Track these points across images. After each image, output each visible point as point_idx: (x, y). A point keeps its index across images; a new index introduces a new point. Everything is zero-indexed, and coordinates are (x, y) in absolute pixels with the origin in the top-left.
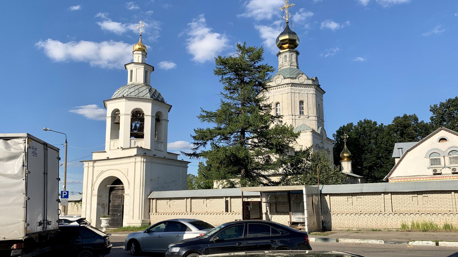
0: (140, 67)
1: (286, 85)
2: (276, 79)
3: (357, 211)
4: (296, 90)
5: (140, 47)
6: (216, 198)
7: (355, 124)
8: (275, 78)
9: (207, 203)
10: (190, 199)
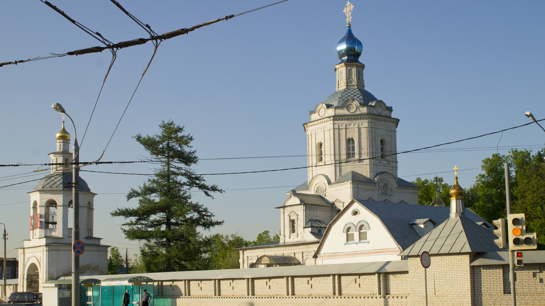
0: (60, 156)
1: (327, 119)
2: (319, 109)
3: (497, 295)
4: (340, 125)
5: (61, 135)
6: (261, 279)
7: (491, 157)
8: (319, 108)
9: (360, 282)
10: (332, 276)
